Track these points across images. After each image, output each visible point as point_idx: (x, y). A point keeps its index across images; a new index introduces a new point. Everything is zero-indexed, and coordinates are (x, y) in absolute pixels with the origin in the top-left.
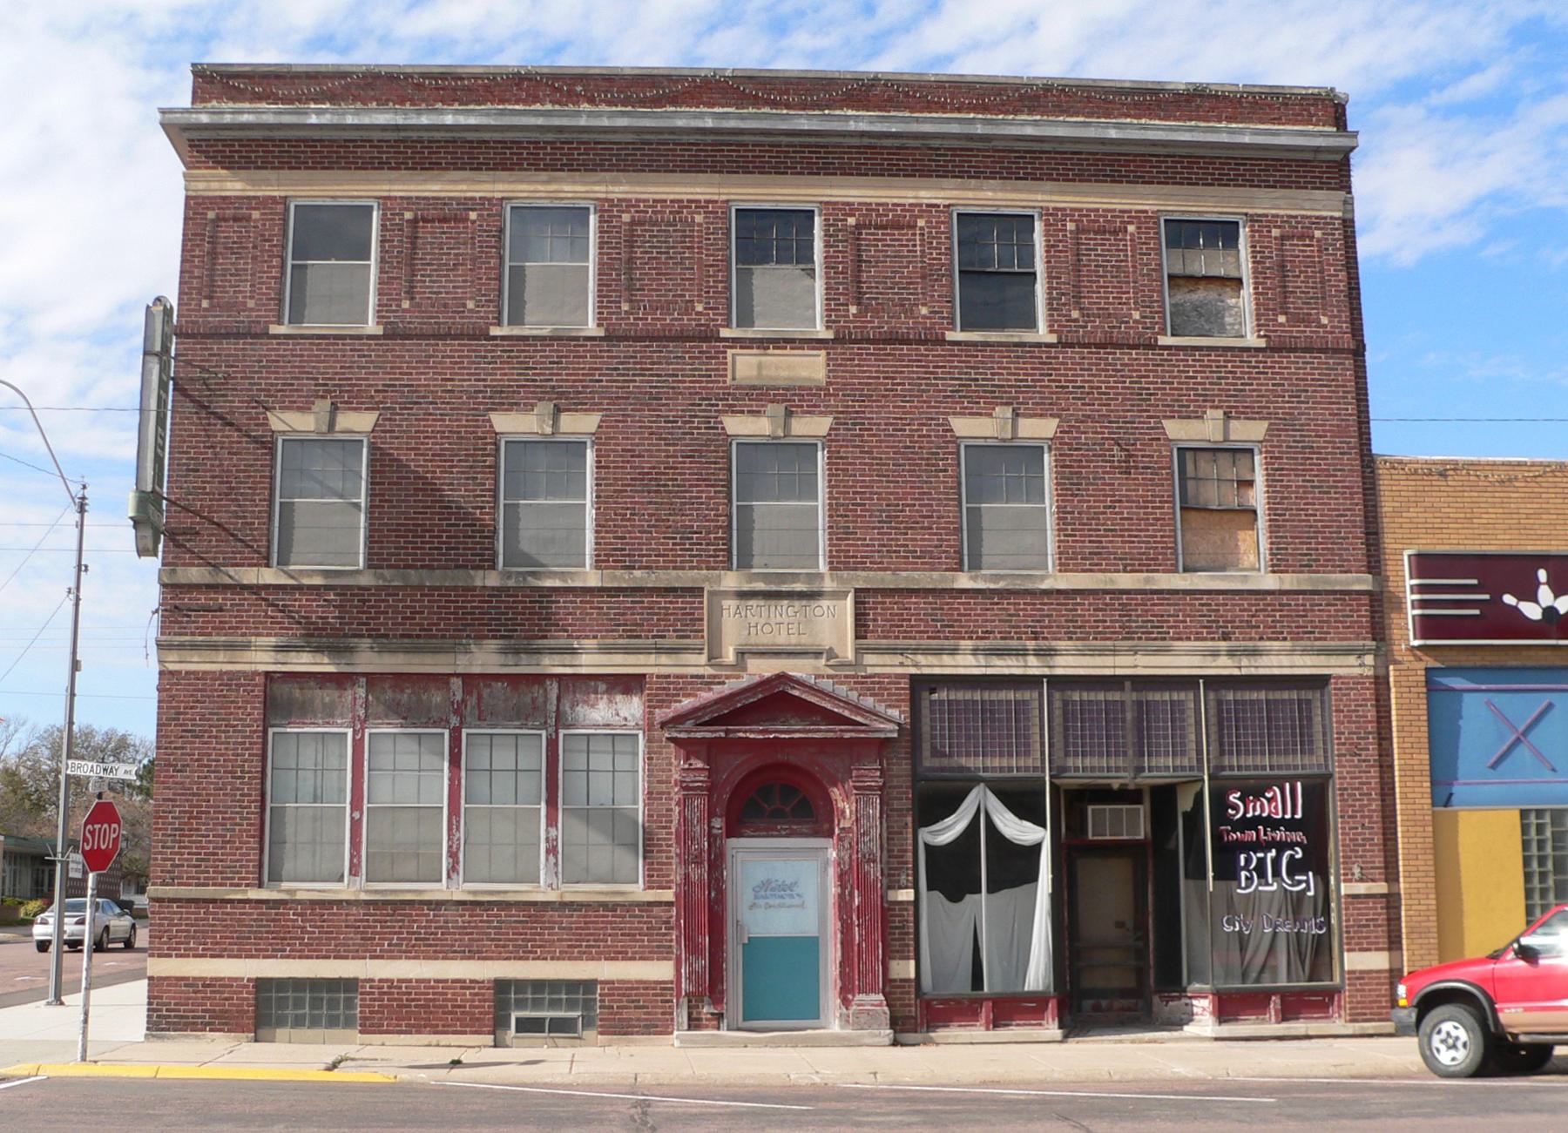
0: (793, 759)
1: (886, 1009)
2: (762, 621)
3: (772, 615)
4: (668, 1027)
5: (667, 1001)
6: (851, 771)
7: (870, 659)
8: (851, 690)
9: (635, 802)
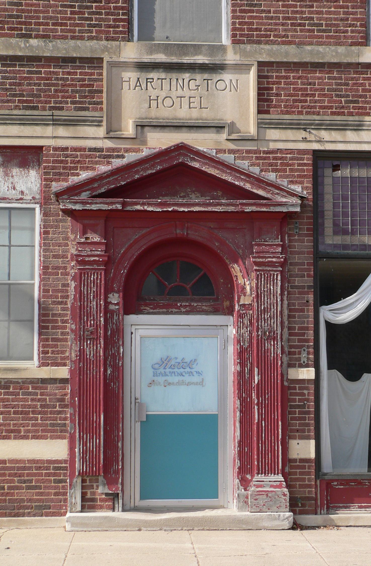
0: (194, 235)
1: (286, 490)
2: (163, 94)
3: (174, 88)
4: (61, 507)
5: (60, 481)
6: (252, 247)
7: (272, 134)
8: (253, 165)
9: (33, 278)
